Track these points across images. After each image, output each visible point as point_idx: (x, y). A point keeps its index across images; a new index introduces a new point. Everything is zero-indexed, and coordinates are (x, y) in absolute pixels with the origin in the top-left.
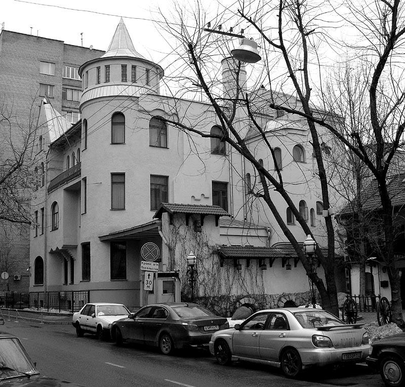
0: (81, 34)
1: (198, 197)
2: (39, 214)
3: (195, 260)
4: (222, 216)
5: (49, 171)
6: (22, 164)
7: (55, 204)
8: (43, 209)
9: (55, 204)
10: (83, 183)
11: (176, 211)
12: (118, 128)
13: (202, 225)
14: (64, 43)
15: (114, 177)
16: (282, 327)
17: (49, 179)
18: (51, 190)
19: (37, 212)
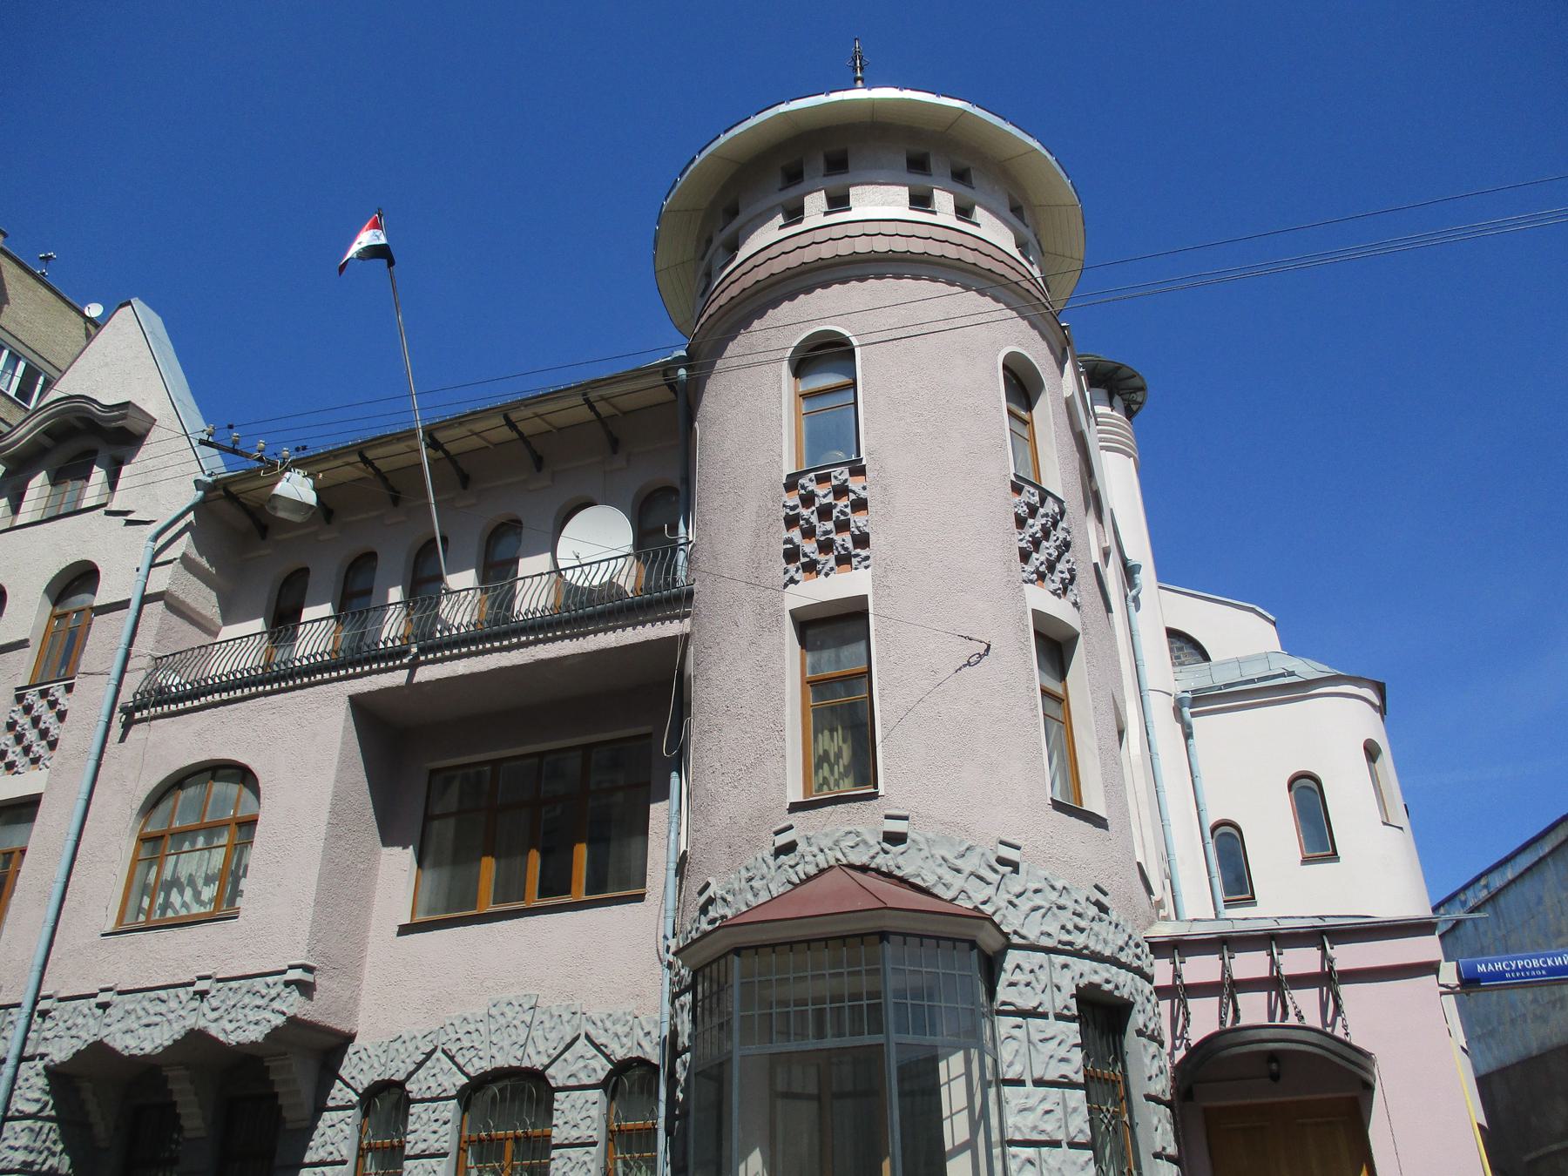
5: (155, 609)
15: (810, 632)
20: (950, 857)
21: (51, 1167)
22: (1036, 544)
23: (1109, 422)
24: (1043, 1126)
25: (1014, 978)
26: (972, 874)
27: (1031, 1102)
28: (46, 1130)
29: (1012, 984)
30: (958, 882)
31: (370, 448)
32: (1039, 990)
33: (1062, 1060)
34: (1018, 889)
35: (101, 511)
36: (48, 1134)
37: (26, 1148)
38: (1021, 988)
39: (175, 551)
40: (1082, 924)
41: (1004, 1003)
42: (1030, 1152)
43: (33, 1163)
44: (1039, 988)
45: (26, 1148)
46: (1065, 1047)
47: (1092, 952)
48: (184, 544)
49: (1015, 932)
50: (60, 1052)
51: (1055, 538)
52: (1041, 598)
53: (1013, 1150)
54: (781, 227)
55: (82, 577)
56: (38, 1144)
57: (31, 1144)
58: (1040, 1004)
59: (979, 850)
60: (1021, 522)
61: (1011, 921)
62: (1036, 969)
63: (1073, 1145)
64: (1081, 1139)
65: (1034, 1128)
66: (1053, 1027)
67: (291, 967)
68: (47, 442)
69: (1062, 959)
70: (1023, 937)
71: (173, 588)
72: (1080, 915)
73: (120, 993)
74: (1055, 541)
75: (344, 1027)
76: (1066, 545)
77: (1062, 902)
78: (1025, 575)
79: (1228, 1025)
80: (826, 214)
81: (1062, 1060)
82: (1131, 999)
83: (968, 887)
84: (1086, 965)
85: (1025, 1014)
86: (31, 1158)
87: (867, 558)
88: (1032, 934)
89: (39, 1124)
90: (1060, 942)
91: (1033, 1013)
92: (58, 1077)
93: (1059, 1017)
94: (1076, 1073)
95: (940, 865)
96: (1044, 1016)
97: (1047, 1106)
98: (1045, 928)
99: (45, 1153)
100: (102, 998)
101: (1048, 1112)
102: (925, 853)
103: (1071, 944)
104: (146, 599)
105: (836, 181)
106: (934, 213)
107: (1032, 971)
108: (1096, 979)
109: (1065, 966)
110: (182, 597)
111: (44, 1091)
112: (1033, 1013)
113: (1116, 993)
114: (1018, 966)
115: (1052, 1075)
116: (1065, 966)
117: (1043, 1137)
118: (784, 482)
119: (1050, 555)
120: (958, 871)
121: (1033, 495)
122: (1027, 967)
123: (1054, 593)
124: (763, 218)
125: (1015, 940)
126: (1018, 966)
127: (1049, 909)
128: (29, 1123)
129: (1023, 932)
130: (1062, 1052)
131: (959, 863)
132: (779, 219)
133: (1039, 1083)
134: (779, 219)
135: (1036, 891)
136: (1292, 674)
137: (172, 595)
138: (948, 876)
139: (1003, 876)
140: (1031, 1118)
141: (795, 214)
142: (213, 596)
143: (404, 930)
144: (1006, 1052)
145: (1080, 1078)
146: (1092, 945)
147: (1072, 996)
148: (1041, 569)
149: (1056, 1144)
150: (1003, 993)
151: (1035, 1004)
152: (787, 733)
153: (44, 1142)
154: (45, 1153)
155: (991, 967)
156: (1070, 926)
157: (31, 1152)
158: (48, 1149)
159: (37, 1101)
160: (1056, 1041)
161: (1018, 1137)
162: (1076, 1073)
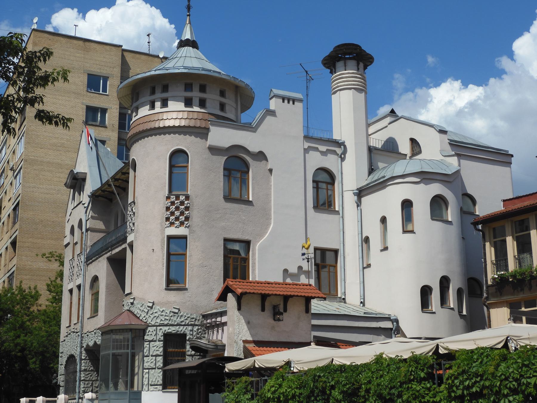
0: (148, 35)
1: (293, 270)
2: (75, 291)
3: (196, 328)
4: (314, 298)
5: (89, 232)
6: (518, 400)
7: (95, 279)
8: (79, 287)
9: (95, 279)
10: (128, 251)
11: (245, 291)
12: (526, 256)
13: (285, 310)
14: (123, 47)
15: (171, 240)
16: (188, 372)
17: (89, 243)
18: (90, 259)
19: (71, 291)
20: (139, 307)
21: (91, 369)
23: (339, 78)
24: (150, 365)
25: (148, 334)
26: (143, 310)
27: (149, 360)
28: (88, 362)
29: (148, 335)
30: (140, 312)
31: (115, 176)
32: (153, 336)
33: (157, 351)
34: (152, 313)
35: (81, 204)
36: (89, 363)
37: (84, 366)
38: (150, 336)
39: (90, 217)
40: (167, 318)
41: (146, 339)
42: (147, 371)
43: (87, 369)
44: (153, 335)
45: (84, 366)
46: (158, 348)
47: (170, 324)
48: (91, 214)
49: (150, 323)
50: (85, 345)
52: (173, 231)
53: (144, 370)
54: (135, 116)
56: (87, 365)
57: (85, 365)
58: (153, 339)
59: (145, 305)
60: (168, 209)
61: (149, 321)
62: (153, 331)
63: (159, 369)
64: (159, 367)
69: (160, 327)
70: (151, 324)
71: (91, 226)
72: (167, 316)
73: (90, 332)
76: (187, 208)
77: (162, 314)
78: (166, 225)
79: (512, 266)
80: (161, 108)
81: (157, 351)
82: (185, 333)
83: (142, 314)
84: (166, 329)
85: (150, 341)
86: (86, 368)
87: (134, 230)
88: (153, 323)
89: (86, 361)
90: (160, 324)
91: (152, 341)
92: (85, 350)
93: (159, 341)
94: (160, 353)
95: (138, 309)
96: (155, 341)
97: (152, 361)
98: (157, 321)
99: (89, 367)
100: (95, 331)
101: (152, 362)
102: (136, 307)
103: (164, 324)
105: (165, 95)
106: (226, 113)
107: (152, 332)
108: (170, 331)
109: (161, 329)
110: (94, 227)
111: (85, 354)
112: (152, 341)
113: (178, 333)
114: (149, 331)
115: (154, 354)
116: (161, 329)
118: (167, 195)
119: (177, 216)
120: (141, 310)
121: (173, 198)
122: (151, 331)
123: (176, 227)
124: (143, 105)
125: (150, 325)
126: (149, 331)
127: (158, 316)
128: (84, 361)
129: (151, 323)
130: (157, 349)
131: (141, 308)
132: (148, 107)
133: (152, 356)
134: (148, 107)
135: (156, 312)
136: (384, 177)
137: (91, 228)
138: (139, 311)
139: (148, 310)
140: (149, 363)
141: (153, 107)
142: (101, 223)
144: (145, 351)
145: (162, 354)
146: (170, 323)
147: (161, 336)
148: (172, 221)
149: (155, 369)
150: (146, 337)
151: (152, 339)
152: (523, 218)
153: (89, 364)
154: (89, 367)
155: (143, 331)
156: (163, 319)
157: (86, 367)
158: (90, 366)
159: (84, 356)
161: (146, 368)
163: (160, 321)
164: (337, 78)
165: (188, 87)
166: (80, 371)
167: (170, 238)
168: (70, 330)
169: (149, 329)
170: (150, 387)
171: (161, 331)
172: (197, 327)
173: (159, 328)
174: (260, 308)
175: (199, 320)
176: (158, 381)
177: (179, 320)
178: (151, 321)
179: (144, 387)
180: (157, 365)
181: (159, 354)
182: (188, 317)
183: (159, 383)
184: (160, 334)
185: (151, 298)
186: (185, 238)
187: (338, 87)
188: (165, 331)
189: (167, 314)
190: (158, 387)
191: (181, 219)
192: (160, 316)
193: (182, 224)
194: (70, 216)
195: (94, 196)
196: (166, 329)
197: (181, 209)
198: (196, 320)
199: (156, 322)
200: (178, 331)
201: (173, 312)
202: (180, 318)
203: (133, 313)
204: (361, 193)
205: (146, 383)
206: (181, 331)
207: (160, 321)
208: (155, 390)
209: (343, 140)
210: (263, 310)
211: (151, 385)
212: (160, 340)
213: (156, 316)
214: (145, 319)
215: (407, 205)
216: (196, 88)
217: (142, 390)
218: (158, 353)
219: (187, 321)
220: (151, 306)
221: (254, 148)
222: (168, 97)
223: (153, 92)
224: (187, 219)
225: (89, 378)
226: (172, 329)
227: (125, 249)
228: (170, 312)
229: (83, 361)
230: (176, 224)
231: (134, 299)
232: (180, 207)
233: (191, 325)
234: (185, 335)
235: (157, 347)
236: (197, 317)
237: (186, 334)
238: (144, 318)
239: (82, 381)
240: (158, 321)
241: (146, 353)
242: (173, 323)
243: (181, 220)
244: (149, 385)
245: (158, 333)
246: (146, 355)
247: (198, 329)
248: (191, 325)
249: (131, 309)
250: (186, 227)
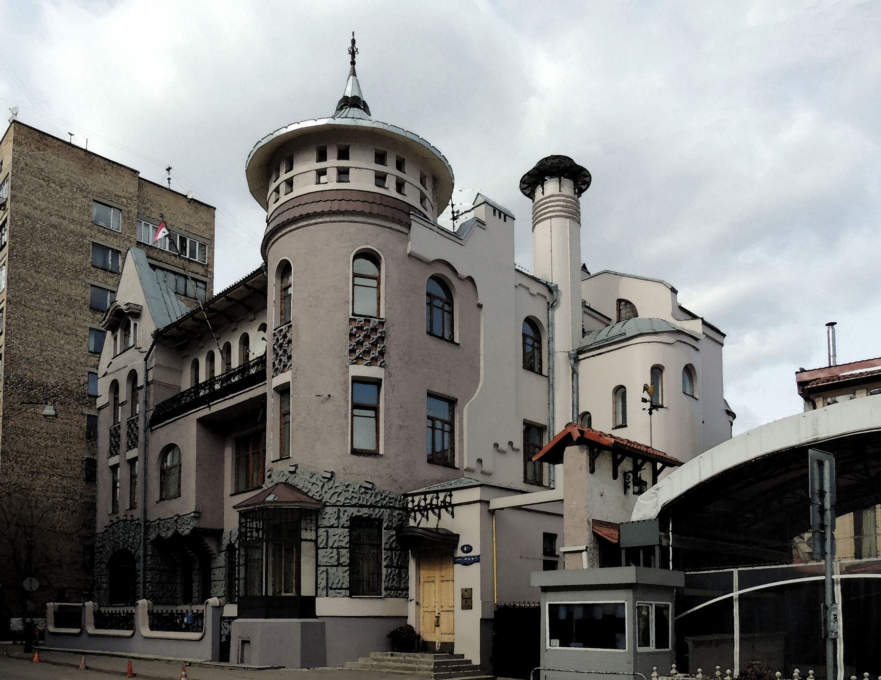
22: (360, 343)
24: (329, 561)
35: (133, 348)
42: (324, 568)
51: (371, 339)
55: (133, 376)
58: (333, 524)
60: (352, 335)
65: (326, 562)
66: (339, 531)
67: (192, 512)
68: (116, 319)
74: (372, 340)
75: (219, 528)
93: (343, 527)
104: (148, 383)
115: (335, 546)
117: (330, 564)
125: (327, 504)
129: (329, 501)
136: (625, 334)
143: (231, 495)
145: (348, 546)
160: (339, 535)
162: (346, 544)
163: (345, 500)
164: (551, 199)
165: (380, 158)
166: (145, 570)
167: (356, 380)
168: (117, 518)
169: (328, 509)
170: (330, 591)
171: (346, 514)
172: (398, 511)
173: (342, 509)
174: (610, 474)
175: (400, 501)
176: (343, 583)
177: (372, 500)
178: (330, 499)
179: (319, 591)
180: (341, 562)
181: (344, 545)
182: (387, 496)
183: (344, 587)
184: (344, 519)
185: (325, 465)
186: (377, 383)
187: (545, 214)
188: (353, 513)
189: (355, 490)
190: (343, 591)
191: (373, 354)
192: (343, 492)
193: (375, 359)
194: (108, 367)
195: (159, 337)
196: (354, 511)
197: (374, 338)
198: (396, 500)
199: (338, 501)
200: (372, 515)
201: (366, 488)
202: (375, 497)
203: (294, 488)
204: (576, 356)
205: (323, 584)
206: (377, 514)
207: (345, 500)
208: (338, 595)
209: (555, 282)
210: (615, 477)
211: (331, 589)
212: (344, 526)
213: (336, 493)
214: (319, 496)
215: (657, 371)
216: (391, 161)
217: (316, 595)
218: (342, 544)
219: (385, 502)
220: (330, 477)
221: (463, 272)
222: (350, 167)
223: (322, 157)
224: (382, 353)
225: (158, 579)
226: (364, 512)
227: (264, 396)
228: (361, 487)
229: (149, 558)
230: (365, 360)
231: (296, 466)
232: (372, 336)
233: (390, 507)
234: (380, 521)
235: (339, 536)
236: (397, 496)
237: (383, 520)
238: (318, 494)
239: (149, 582)
240: (342, 499)
241: (321, 543)
242: (364, 503)
243: (374, 356)
244: (329, 589)
245: (341, 515)
246: (321, 546)
247: (399, 514)
248: (390, 507)
249: (290, 481)
250: (380, 366)
